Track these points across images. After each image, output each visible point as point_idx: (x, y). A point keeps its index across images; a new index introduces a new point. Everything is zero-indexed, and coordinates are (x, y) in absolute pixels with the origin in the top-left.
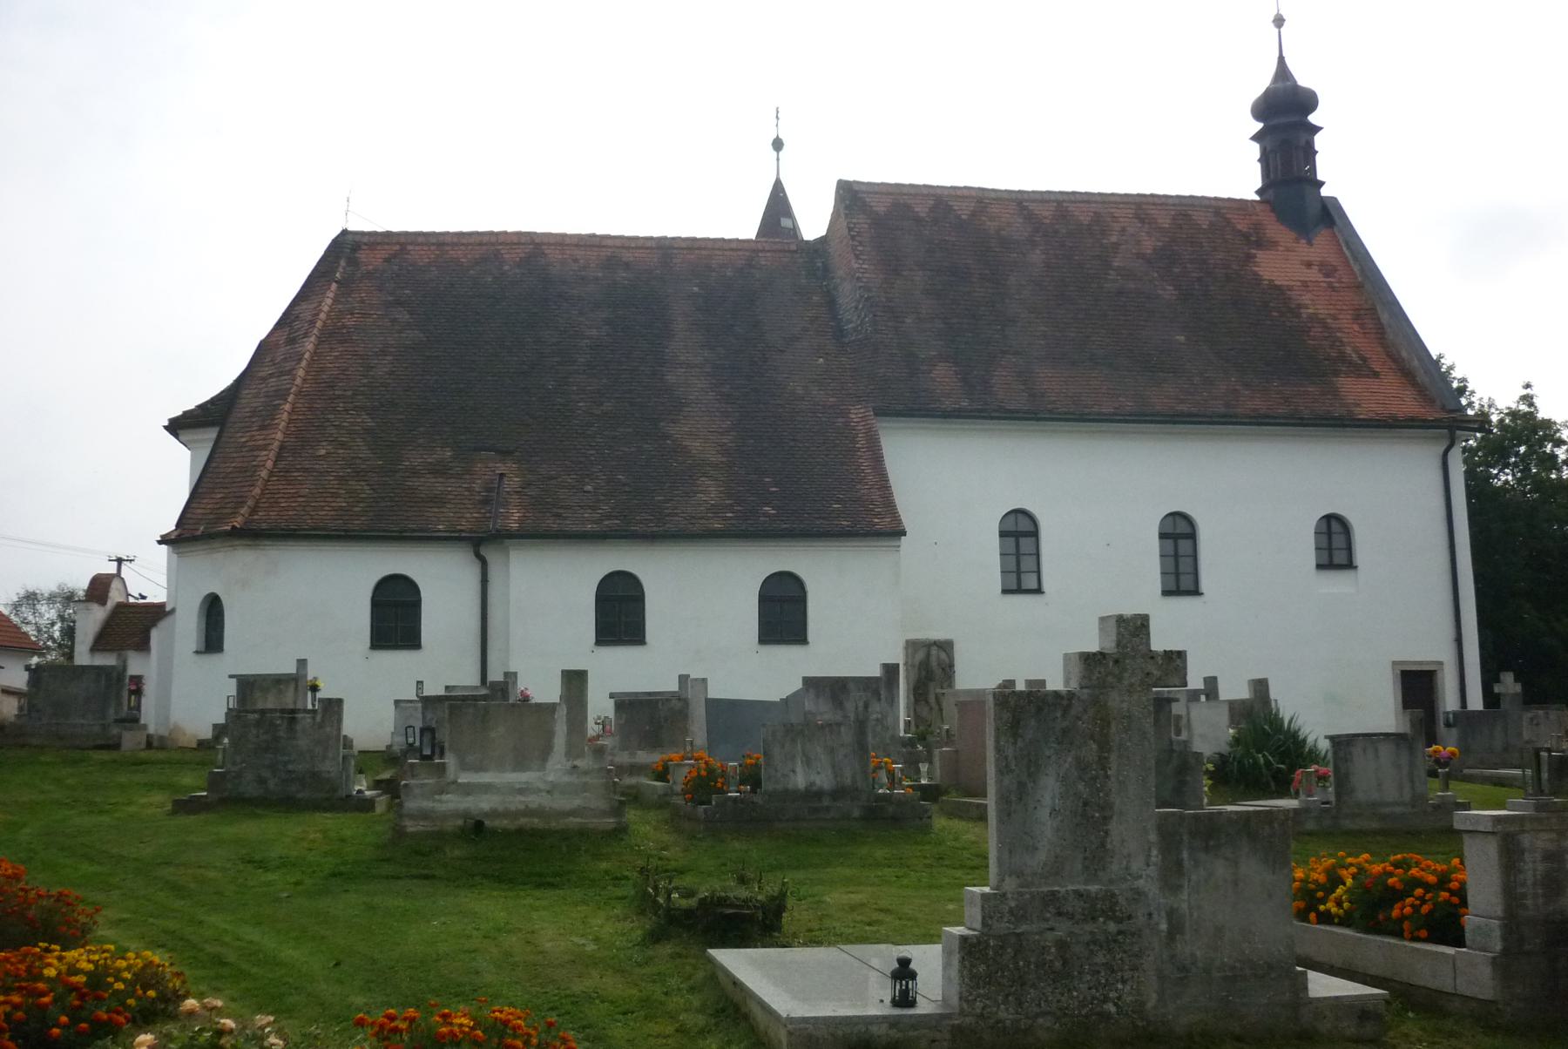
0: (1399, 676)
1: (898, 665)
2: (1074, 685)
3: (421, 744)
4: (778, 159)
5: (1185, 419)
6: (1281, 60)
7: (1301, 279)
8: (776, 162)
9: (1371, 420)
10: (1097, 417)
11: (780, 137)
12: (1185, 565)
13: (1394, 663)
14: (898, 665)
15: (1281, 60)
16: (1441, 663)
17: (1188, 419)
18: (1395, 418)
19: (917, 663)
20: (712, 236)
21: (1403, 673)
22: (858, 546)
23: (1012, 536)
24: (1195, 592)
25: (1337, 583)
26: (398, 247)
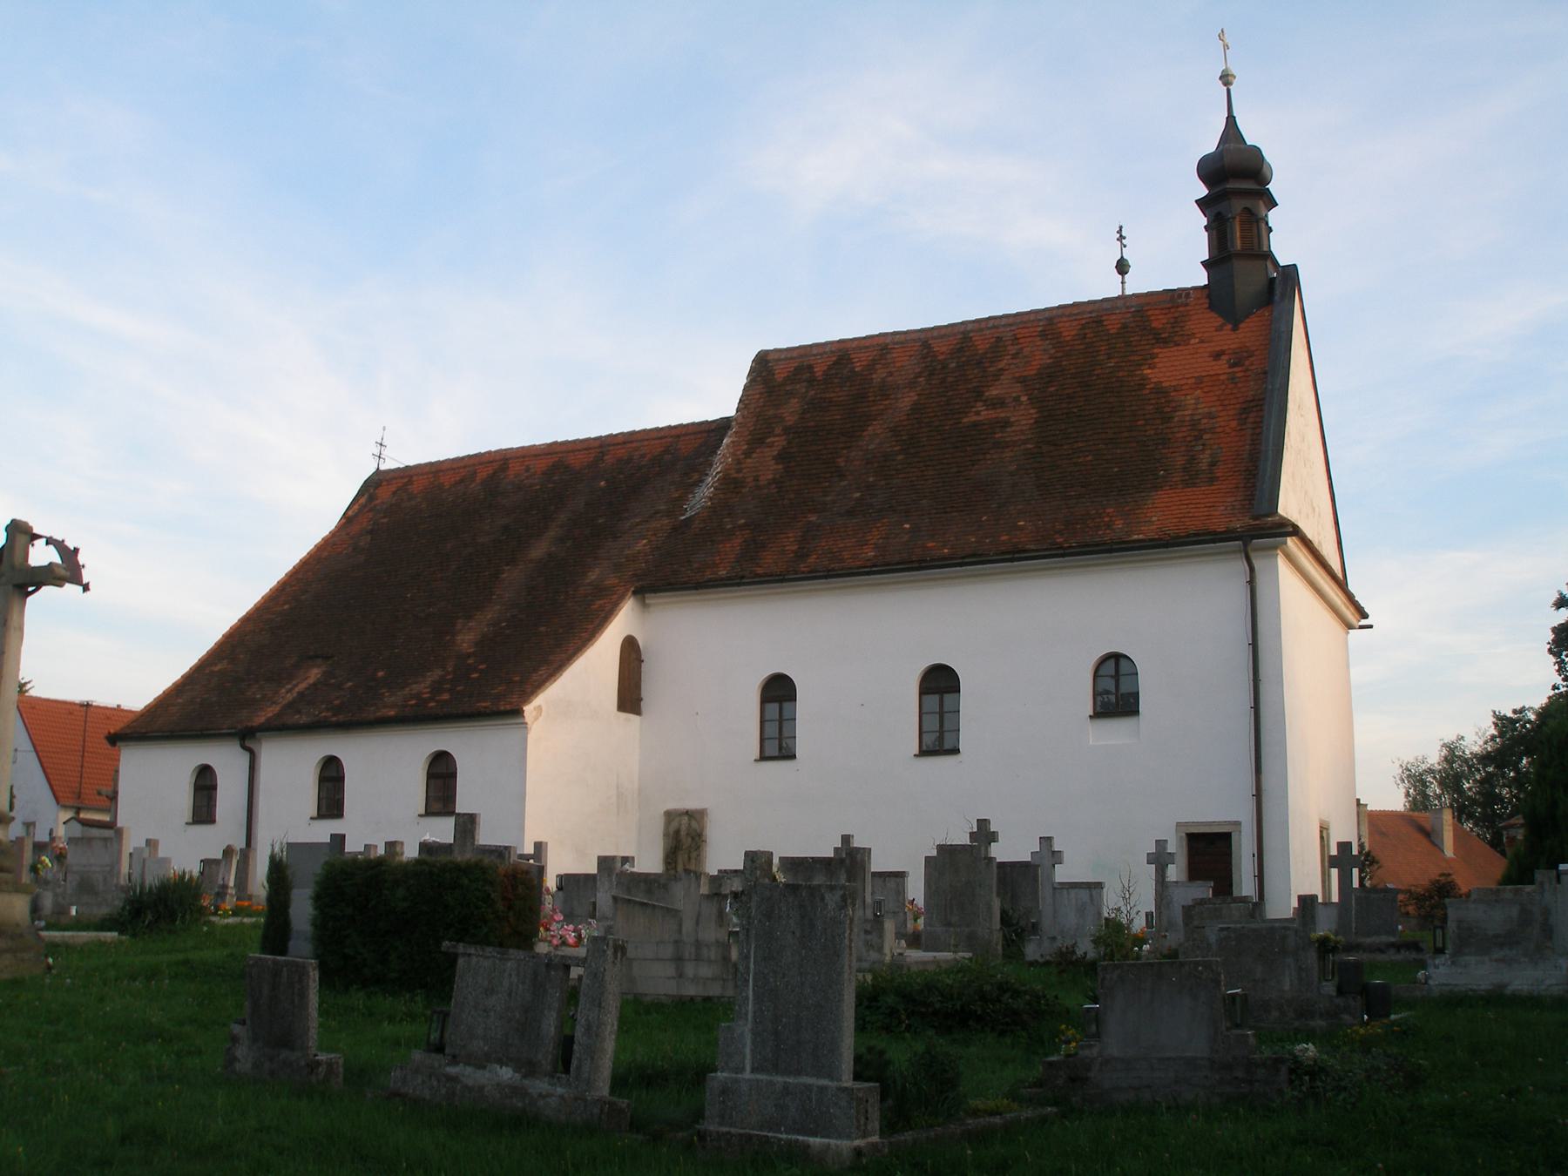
0: (1185, 843)
1: (1351, 843)
2: (347, 855)
3: (1444, 943)
4: (1123, 283)
5: (937, 563)
6: (1231, 120)
7: (1196, 375)
8: (1121, 285)
9: (1151, 540)
10: (840, 572)
11: (1125, 257)
12: (772, 730)
13: (1178, 824)
14: (1351, 843)
15: (1231, 120)
16: (1238, 824)
17: (940, 563)
18: (1215, 533)
19: (671, 833)
20: (582, 437)
21: (1226, 837)
22: (502, 725)
23: (775, 701)
24: (793, 757)
25: (1116, 731)
26: (406, 480)
